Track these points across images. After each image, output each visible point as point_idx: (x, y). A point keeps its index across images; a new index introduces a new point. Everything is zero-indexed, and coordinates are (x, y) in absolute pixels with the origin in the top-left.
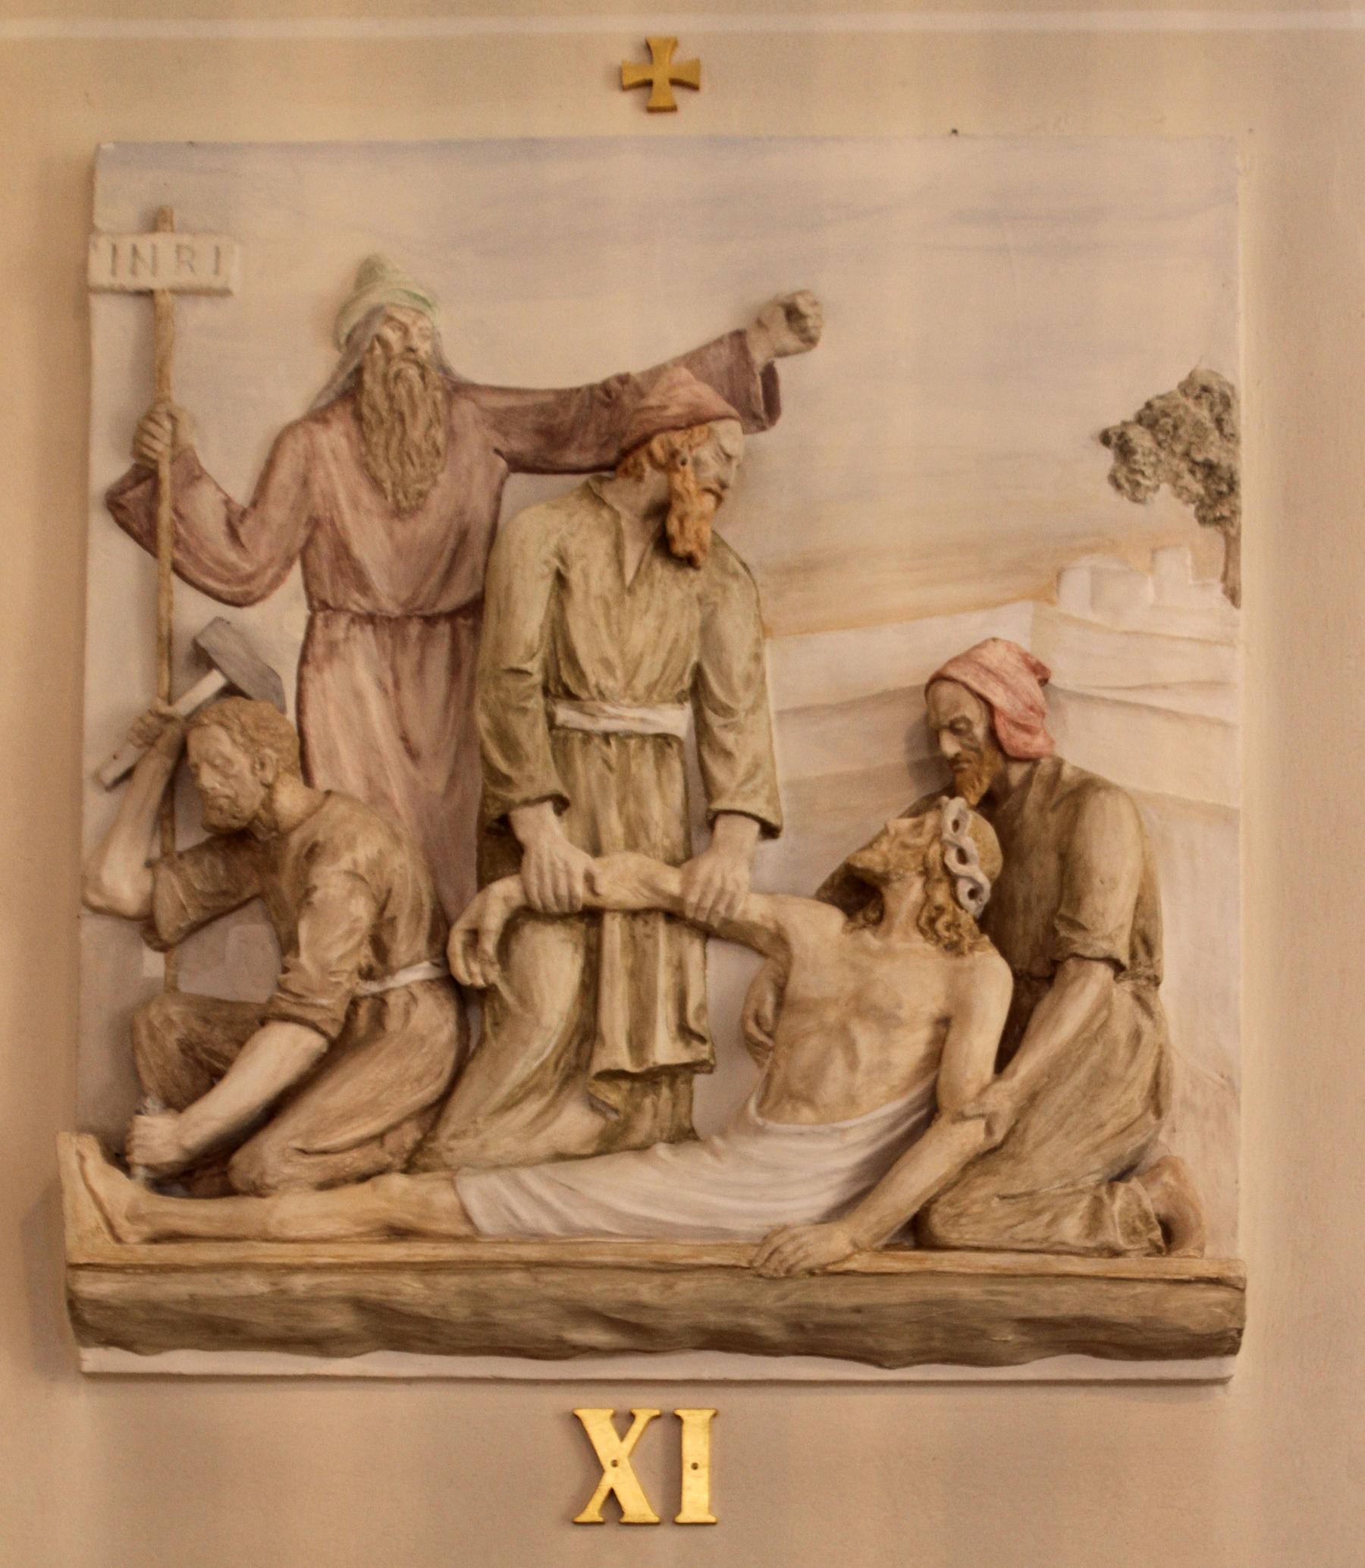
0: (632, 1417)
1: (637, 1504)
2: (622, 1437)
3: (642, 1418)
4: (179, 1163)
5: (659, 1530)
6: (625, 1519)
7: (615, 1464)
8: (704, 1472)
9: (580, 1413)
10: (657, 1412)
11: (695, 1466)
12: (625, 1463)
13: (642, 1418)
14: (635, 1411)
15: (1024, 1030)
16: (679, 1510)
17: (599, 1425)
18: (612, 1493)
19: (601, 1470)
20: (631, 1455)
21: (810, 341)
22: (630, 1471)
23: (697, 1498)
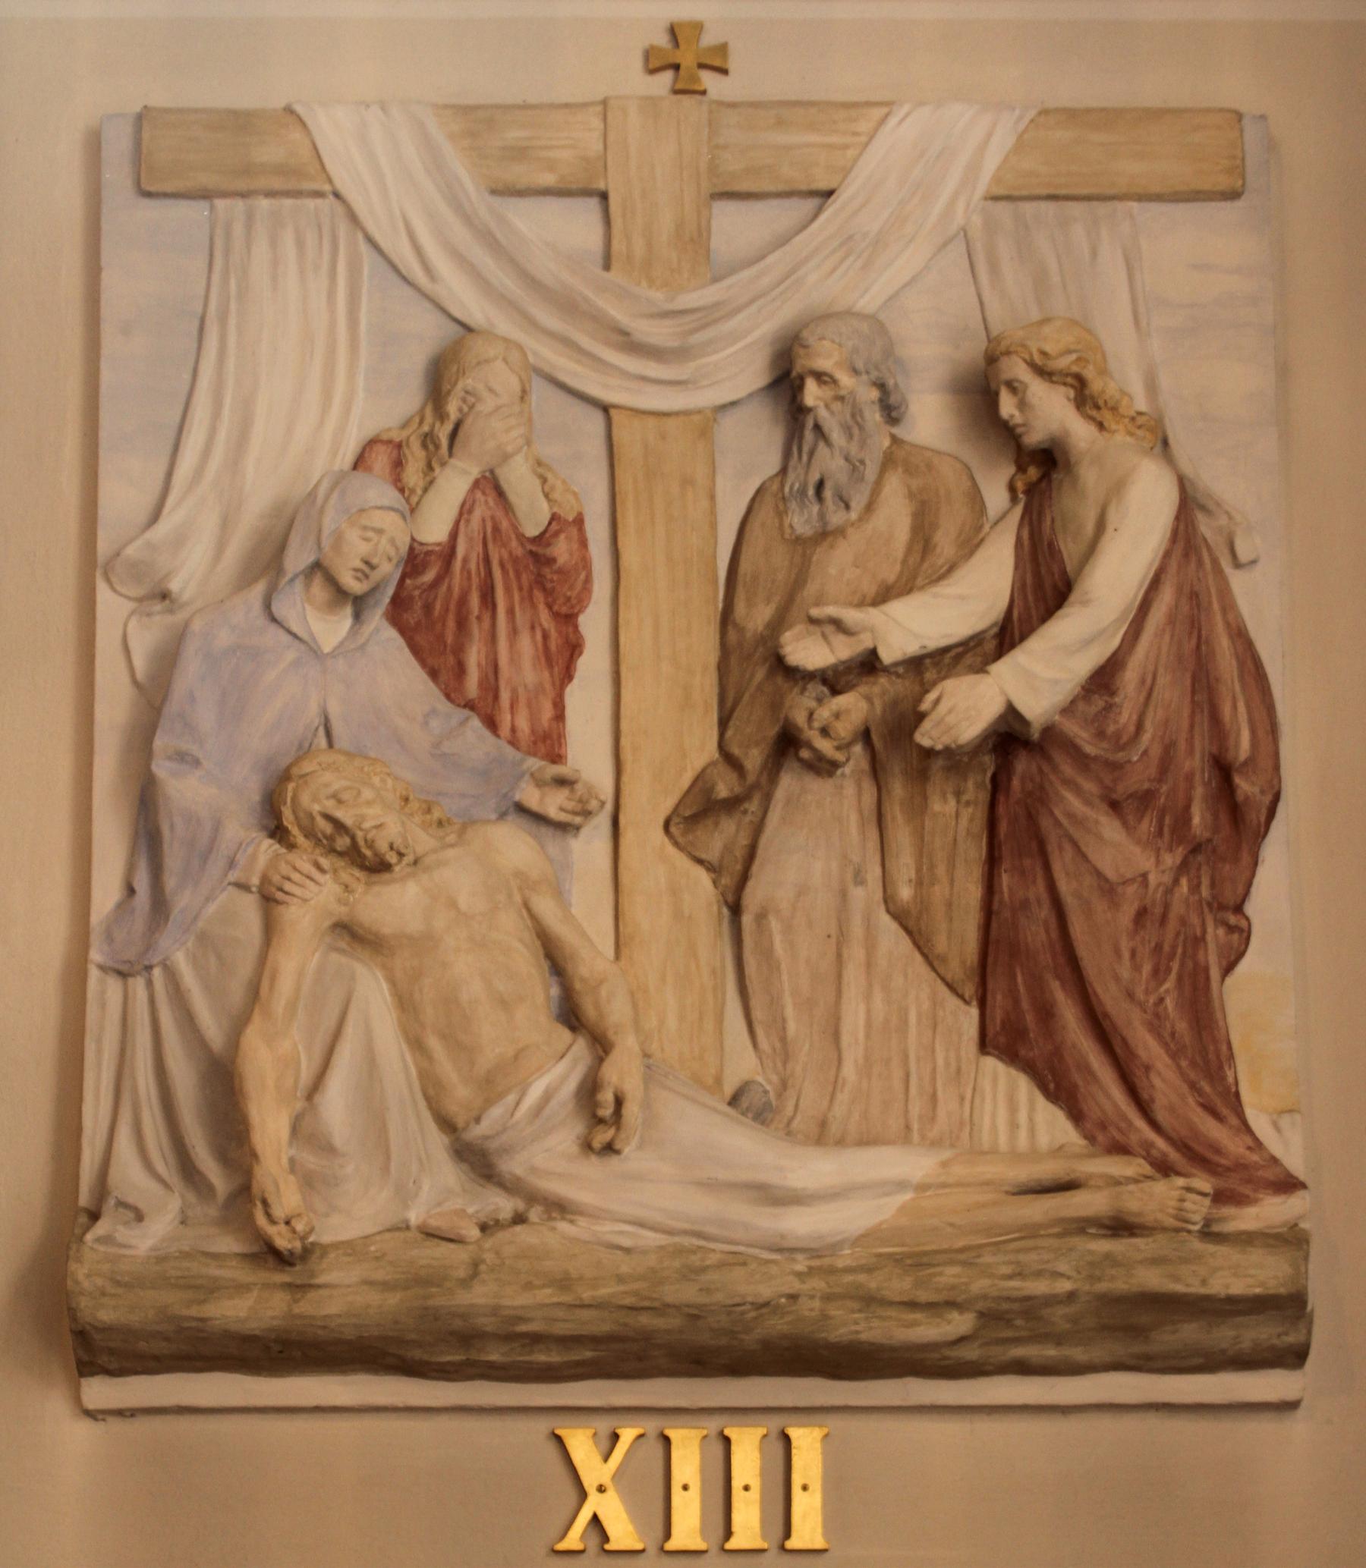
1: (622, 1533)
11: (746, 1488)
17: (581, 1445)
18: (595, 1519)
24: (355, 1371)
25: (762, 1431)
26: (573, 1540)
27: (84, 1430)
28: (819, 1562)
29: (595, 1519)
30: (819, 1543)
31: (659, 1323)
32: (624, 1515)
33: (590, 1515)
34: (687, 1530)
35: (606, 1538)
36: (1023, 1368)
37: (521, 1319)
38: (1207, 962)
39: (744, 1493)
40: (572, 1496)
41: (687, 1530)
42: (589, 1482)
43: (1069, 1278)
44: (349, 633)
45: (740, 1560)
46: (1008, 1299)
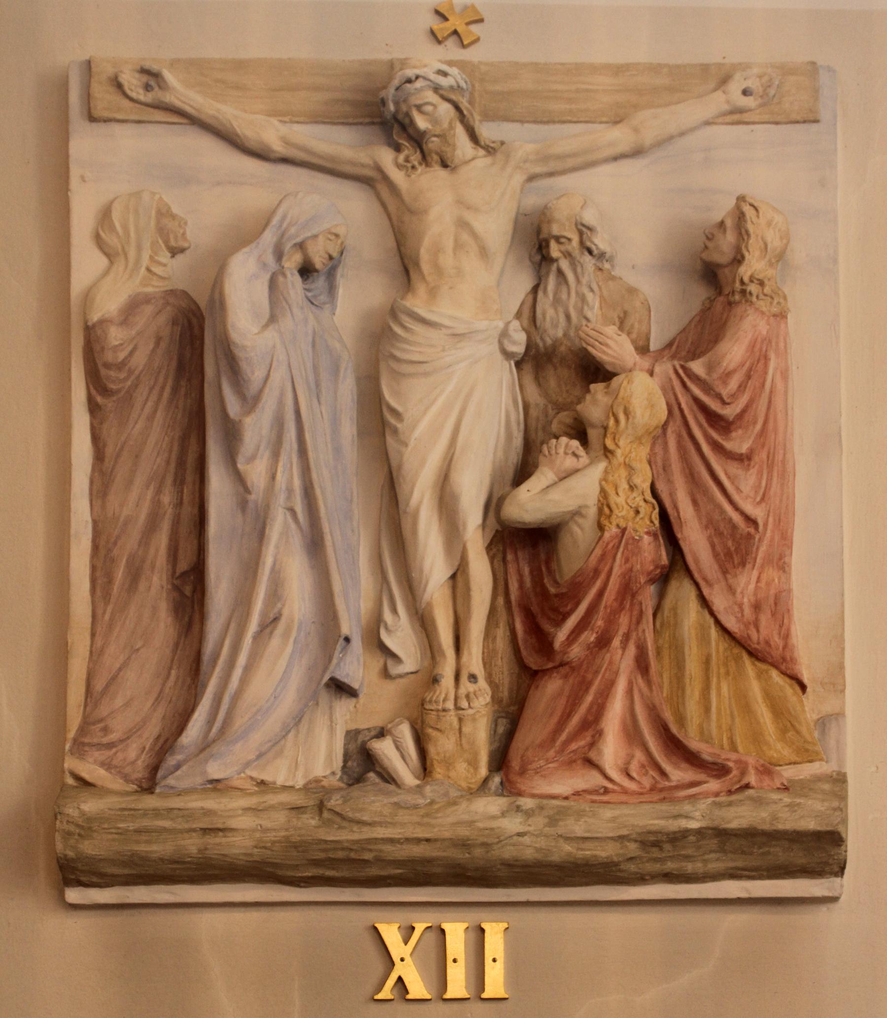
0: (413, 928)
1: (417, 988)
2: (406, 942)
3: (420, 928)
4: (499, 747)
5: (466, 1004)
6: (409, 997)
7: (402, 960)
8: (500, 965)
9: (376, 925)
10: (430, 925)
11: (455, 961)
12: (408, 959)
13: (420, 928)
14: (414, 925)
15: (515, 655)
16: (483, 990)
17: (391, 934)
18: (400, 979)
19: (393, 964)
20: (411, 954)
21: (741, 199)
22: (413, 967)
23: (495, 981)
24: (244, 881)
25: (465, 925)
26: (386, 993)
27: (77, 927)
28: (502, 1005)
29: (400, 979)
30: (501, 994)
31: (238, 862)
32: (420, 979)
33: (397, 977)
34: (458, 983)
35: (407, 992)
36: (669, 877)
37: (468, 840)
38: (645, 639)
39: (497, 957)
40: (379, 966)
41: (458, 983)
42: (396, 959)
43: (697, 820)
44: (518, 372)
45: (455, 1006)
46: (650, 832)
